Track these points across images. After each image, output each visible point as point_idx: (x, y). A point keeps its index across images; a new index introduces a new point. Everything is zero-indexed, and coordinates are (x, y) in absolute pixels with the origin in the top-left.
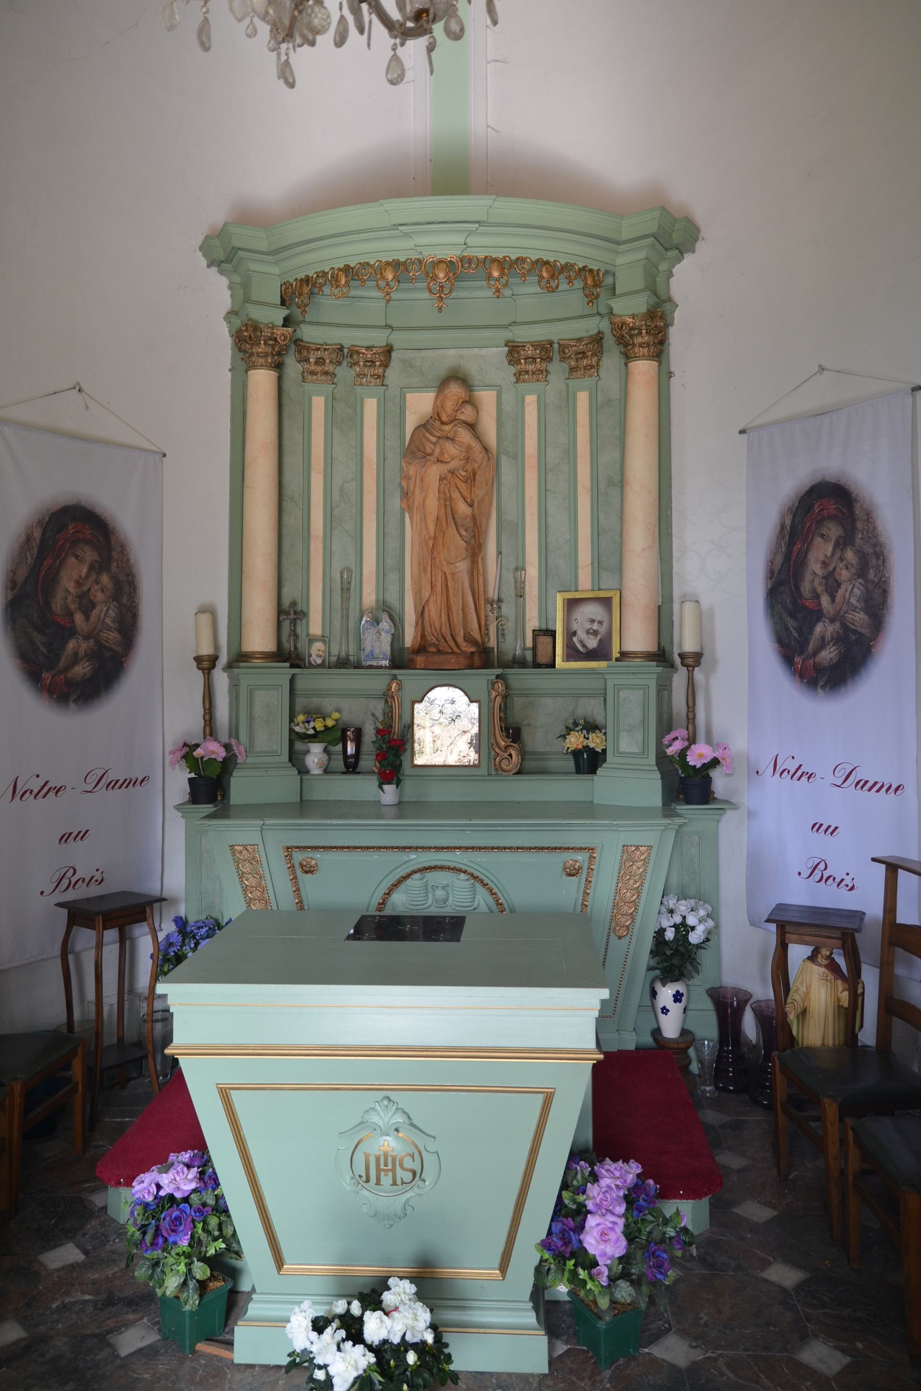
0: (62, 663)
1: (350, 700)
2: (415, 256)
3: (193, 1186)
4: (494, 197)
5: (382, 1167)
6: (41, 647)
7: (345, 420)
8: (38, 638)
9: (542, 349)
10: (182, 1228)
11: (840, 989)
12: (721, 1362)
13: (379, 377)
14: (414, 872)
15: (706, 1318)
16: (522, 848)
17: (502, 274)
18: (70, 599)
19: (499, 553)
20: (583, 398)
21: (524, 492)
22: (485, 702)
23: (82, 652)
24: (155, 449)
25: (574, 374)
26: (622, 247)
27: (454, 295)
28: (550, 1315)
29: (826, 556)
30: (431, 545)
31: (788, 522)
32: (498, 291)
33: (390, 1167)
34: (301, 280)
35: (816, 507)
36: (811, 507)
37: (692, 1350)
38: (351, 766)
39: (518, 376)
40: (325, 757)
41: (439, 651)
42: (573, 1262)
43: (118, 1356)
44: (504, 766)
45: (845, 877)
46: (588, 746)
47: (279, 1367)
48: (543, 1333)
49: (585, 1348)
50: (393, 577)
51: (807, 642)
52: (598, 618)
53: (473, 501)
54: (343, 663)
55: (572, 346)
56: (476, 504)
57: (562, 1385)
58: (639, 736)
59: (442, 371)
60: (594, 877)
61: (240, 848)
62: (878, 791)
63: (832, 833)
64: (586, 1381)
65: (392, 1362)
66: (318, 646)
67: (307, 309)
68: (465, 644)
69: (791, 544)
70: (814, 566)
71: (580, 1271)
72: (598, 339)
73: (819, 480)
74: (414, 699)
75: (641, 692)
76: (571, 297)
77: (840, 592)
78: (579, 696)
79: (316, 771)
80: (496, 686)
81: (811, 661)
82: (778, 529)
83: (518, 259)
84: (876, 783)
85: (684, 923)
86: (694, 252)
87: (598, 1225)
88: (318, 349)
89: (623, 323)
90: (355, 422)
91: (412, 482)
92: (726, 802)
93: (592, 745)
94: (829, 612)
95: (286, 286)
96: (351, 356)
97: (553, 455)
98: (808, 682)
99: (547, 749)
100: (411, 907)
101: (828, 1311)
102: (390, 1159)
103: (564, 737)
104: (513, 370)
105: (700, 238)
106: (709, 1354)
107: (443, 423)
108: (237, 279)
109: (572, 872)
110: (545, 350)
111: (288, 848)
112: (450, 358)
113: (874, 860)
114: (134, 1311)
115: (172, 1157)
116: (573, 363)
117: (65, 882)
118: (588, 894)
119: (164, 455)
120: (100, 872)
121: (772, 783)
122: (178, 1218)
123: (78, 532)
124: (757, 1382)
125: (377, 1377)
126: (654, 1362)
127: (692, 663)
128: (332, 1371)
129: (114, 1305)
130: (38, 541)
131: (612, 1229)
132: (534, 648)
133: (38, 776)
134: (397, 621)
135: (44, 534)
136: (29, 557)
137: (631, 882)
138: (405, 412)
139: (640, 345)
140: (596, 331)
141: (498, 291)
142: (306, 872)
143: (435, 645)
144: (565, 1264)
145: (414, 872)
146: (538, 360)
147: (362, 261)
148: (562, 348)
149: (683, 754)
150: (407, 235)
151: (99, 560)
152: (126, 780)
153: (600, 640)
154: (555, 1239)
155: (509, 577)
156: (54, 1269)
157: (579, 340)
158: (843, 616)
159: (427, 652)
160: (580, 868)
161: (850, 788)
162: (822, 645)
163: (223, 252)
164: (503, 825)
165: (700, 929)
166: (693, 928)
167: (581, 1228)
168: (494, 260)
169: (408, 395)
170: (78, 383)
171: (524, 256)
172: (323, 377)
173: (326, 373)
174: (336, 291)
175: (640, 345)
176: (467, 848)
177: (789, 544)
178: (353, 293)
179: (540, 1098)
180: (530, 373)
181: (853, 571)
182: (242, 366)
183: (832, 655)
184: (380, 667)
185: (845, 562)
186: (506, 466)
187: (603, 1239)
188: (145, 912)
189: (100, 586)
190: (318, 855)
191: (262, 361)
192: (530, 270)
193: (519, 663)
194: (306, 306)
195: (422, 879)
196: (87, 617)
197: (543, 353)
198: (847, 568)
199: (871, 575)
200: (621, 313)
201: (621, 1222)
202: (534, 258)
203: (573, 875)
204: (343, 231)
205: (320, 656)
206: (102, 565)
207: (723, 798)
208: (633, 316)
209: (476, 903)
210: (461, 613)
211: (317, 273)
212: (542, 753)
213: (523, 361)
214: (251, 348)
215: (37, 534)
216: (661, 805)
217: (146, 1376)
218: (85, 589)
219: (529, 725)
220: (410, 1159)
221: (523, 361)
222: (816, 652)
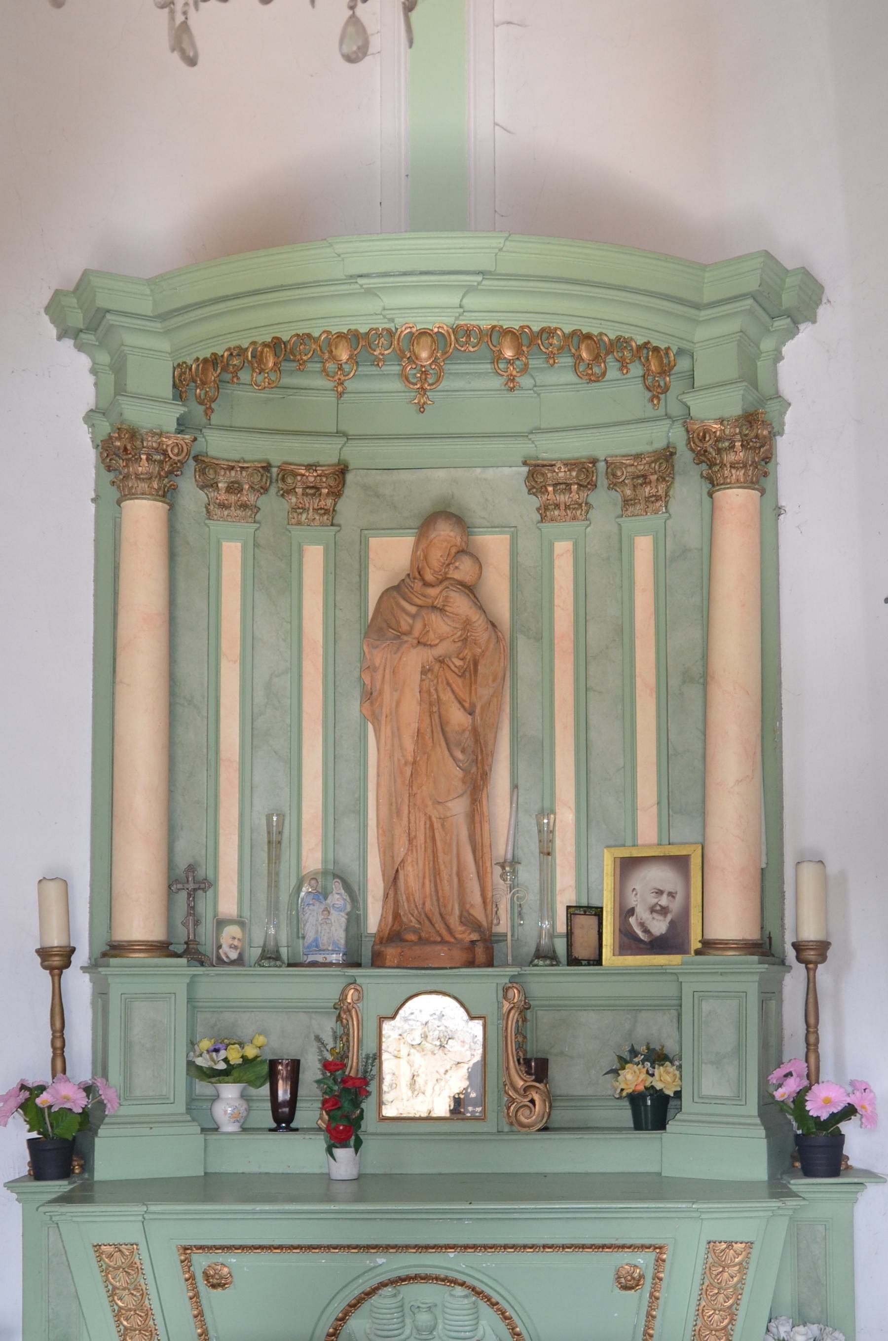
1: (284, 1017)
2: (382, 325)
9: (580, 471)
13: (327, 512)
14: (383, 1285)
17: (519, 353)
19: (515, 787)
20: (643, 549)
22: (492, 1019)
25: (631, 509)
26: (703, 313)
27: (444, 384)
34: (205, 360)
38: (284, 1118)
39: (544, 512)
40: (242, 1106)
44: (523, 1120)
46: (652, 1087)
52: (669, 888)
55: (627, 466)
56: (478, 711)
67: (213, 405)
68: (461, 928)
72: (667, 455)
76: (624, 389)
78: (637, 1009)
80: (510, 994)
83: (543, 330)
88: (232, 468)
91: (378, 676)
93: (659, 1086)
96: (283, 480)
99: (590, 1091)
103: (615, 1072)
104: (535, 502)
105: (824, 300)
107: (427, 584)
108: (104, 358)
109: (628, 1283)
110: (585, 472)
112: (437, 483)
118: (654, 1317)
132: (569, 935)
137: (721, 1298)
138: (367, 567)
142: (214, 1286)
143: (415, 931)
145: (383, 1285)
147: (300, 332)
148: (612, 468)
149: (800, 1098)
150: (370, 292)
153: (672, 924)
155: (529, 824)
157: (638, 457)
160: (642, 1276)
169: (374, 542)
173: (244, 506)
174: (260, 378)
176: (466, 1247)
178: (286, 380)
180: (562, 507)
190: (232, 1259)
191: (143, 486)
192: (561, 348)
194: (213, 400)
195: (395, 1296)
197: (583, 476)
202: (568, 329)
205: (236, 948)
208: (721, 421)
209: (480, 1332)
210: (455, 880)
211: (229, 349)
212: (583, 1098)
213: (550, 489)
214: (127, 466)
219: (562, 1054)
221: (550, 489)
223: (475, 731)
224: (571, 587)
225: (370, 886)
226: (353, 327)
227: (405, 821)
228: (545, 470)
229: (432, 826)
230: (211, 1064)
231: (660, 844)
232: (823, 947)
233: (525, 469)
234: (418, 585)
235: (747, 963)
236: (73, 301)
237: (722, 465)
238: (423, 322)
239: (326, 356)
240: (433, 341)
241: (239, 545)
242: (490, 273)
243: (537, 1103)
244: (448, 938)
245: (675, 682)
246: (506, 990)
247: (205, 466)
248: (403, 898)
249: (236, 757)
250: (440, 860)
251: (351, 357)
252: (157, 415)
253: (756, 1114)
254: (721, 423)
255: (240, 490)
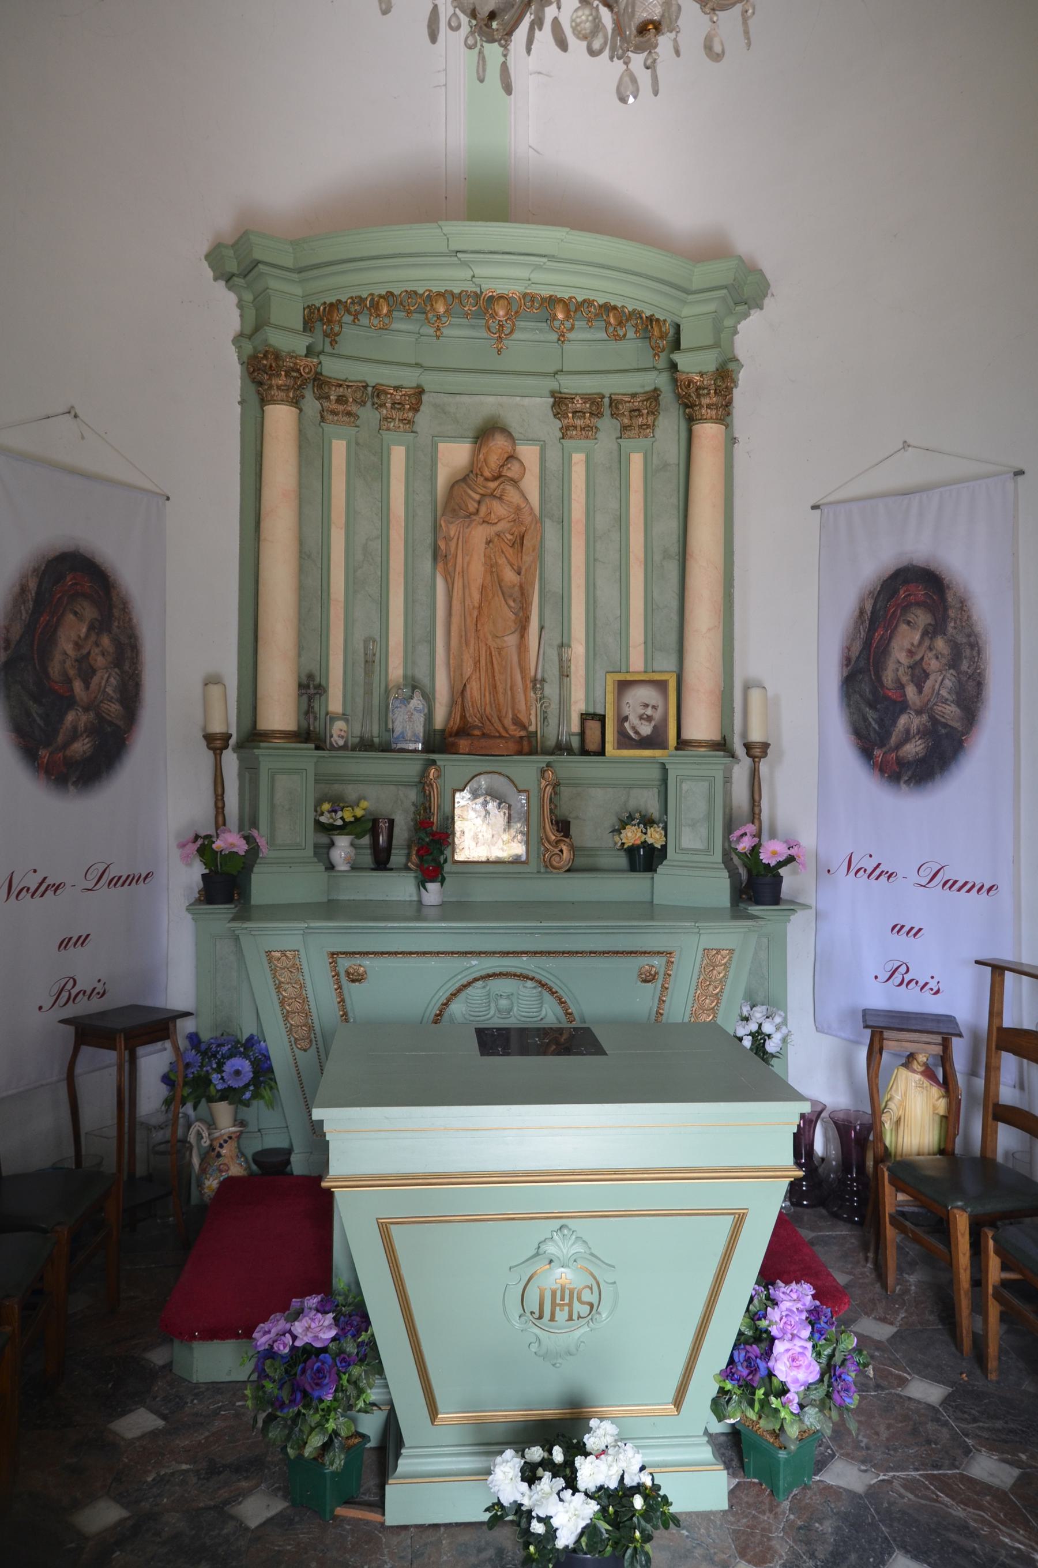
0: (60, 739)
1: (382, 789)
2: (471, 288)
3: (333, 1333)
4: (568, 229)
5: (558, 1301)
6: (38, 719)
7: (370, 470)
8: (34, 708)
9: (592, 404)
10: (326, 1381)
11: (936, 1096)
12: (896, 1483)
13: (409, 422)
14: (476, 980)
15: (865, 1440)
16: (595, 953)
17: (568, 317)
18: (68, 663)
19: (542, 628)
20: (637, 461)
21: (572, 562)
22: (534, 793)
23: (914, 729)
24: (158, 491)
25: (628, 433)
26: (690, 297)
27: (514, 336)
28: (735, 1448)
29: (912, 644)
30: (475, 616)
31: (869, 607)
32: (438, 329)
33: (567, 1301)
34: (331, 305)
35: (901, 592)
36: (895, 592)
37: (863, 1475)
38: (381, 861)
39: (565, 432)
40: (352, 851)
41: (483, 734)
42: (762, 1391)
43: (247, 1529)
44: (555, 863)
45: (929, 980)
46: (645, 841)
47: (482, 1523)
48: (722, 1467)
49: (756, 1481)
50: (423, 649)
51: (889, 734)
52: (653, 702)
53: (520, 568)
54: (365, 745)
55: (626, 402)
56: (523, 573)
57: (745, 1520)
58: (703, 831)
59: (476, 420)
60: (672, 982)
61: (278, 954)
62: (968, 891)
63: (915, 935)
64: (768, 1514)
65: (611, 1508)
66: (339, 726)
67: (337, 338)
68: (513, 727)
69: (871, 630)
70: (899, 653)
71: (773, 1399)
72: (654, 396)
73: (905, 564)
74: (455, 787)
75: (707, 784)
76: (631, 349)
77: (929, 683)
78: (631, 787)
79: (342, 866)
80: (546, 775)
81: (894, 755)
82: (857, 613)
83: (585, 301)
84: (966, 883)
85: (759, 1031)
86: (761, 308)
87: (788, 1350)
88: (341, 386)
89: (690, 382)
90: (381, 472)
91: (453, 544)
92: (792, 902)
93: (650, 841)
94: (914, 703)
95: (310, 309)
96: (378, 396)
97: (602, 521)
98: (890, 777)
99: (596, 844)
100: (472, 1018)
101: (981, 1424)
102: (567, 1292)
103: (618, 831)
104: (558, 424)
105: (769, 295)
106: (881, 1477)
107: (487, 479)
108: (248, 297)
109: (648, 978)
110: (595, 404)
111: (333, 954)
112: (489, 405)
113: (977, 962)
114: (246, 1478)
115: (295, 1303)
116: (626, 421)
117: (65, 995)
118: (664, 1001)
119: (168, 499)
120: (102, 982)
121: (847, 884)
122: (320, 1370)
123: (76, 584)
124: (937, 1501)
125: (603, 1526)
126: (828, 1491)
127: (758, 754)
128: (555, 1522)
129: (219, 1473)
130: (33, 592)
131: (802, 1354)
132: (582, 734)
133: (35, 871)
134: (429, 699)
135: (40, 585)
136: (23, 612)
137: (711, 988)
138: (436, 464)
139: (709, 406)
140: (652, 388)
141: (438, 329)
142: (353, 981)
143: (479, 728)
144: (754, 1394)
145: (476, 980)
146: (588, 415)
147: (409, 289)
148: (614, 403)
149: (755, 850)
150: (466, 264)
151: (933, 623)
152: (128, 876)
153: (655, 727)
154: (740, 1368)
155: (553, 654)
156: (133, 1439)
157: (634, 395)
158: (932, 709)
159: (469, 735)
160: (656, 973)
161: (104, 891)
162: (74, 736)
163: (238, 263)
164: (580, 927)
165: (777, 1037)
166: (769, 1036)
167: (768, 1353)
168: (561, 300)
169: (441, 446)
170: (72, 407)
171: (591, 298)
172: (345, 419)
173: (349, 414)
174: (376, 322)
175: (709, 406)
176: (536, 953)
177: (869, 630)
178: (394, 326)
179: (728, 1221)
180: (579, 429)
181: (944, 661)
182: (254, 399)
183: (85, 747)
184: (415, 751)
185: (934, 652)
186: (550, 531)
187: (794, 1364)
188: (168, 1029)
189: (101, 648)
190: (367, 962)
191: (282, 394)
192: (596, 315)
193: (561, 748)
194: (337, 335)
195: (484, 987)
196: (920, 690)
197: (594, 408)
198: (937, 658)
199: (965, 666)
200: (687, 370)
201: (809, 1345)
202: (601, 301)
203: (649, 981)
204: (392, 252)
205: (342, 737)
206: (101, 625)
207: (788, 898)
208: (701, 374)
209: (543, 1013)
210: (509, 693)
211: (352, 298)
212: (592, 849)
213: (570, 415)
214: (270, 379)
215: (33, 585)
216: (728, 905)
217: (289, 1547)
218: (85, 651)
219: (577, 818)
220: (588, 1290)
221: (570, 415)
222: (66, 745)
223: (521, 587)
224: (584, 487)
225: (438, 695)
226: (449, 289)
227: (472, 650)
228: (567, 401)
229: (491, 654)
230: (331, 821)
231: (645, 672)
232: (765, 746)
233: (552, 400)
234: (480, 479)
235: (716, 756)
236: (231, 253)
237: (271, 387)
238: (501, 288)
239: (428, 308)
240: (509, 303)
241: (344, 442)
242: (553, 256)
243: (565, 852)
244: (504, 734)
245: (657, 557)
246: (543, 772)
247: (319, 381)
248: (468, 704)
249: (342, 598)
250: (497, 678)
251: (446, 311)
252: (291, 342)
253: (721, 861)
254: (701, 376)
255: (346, 402)
